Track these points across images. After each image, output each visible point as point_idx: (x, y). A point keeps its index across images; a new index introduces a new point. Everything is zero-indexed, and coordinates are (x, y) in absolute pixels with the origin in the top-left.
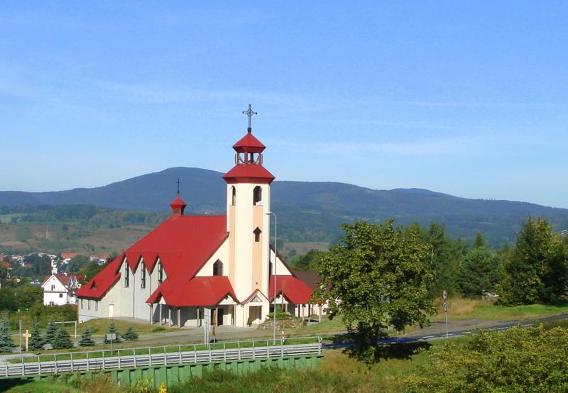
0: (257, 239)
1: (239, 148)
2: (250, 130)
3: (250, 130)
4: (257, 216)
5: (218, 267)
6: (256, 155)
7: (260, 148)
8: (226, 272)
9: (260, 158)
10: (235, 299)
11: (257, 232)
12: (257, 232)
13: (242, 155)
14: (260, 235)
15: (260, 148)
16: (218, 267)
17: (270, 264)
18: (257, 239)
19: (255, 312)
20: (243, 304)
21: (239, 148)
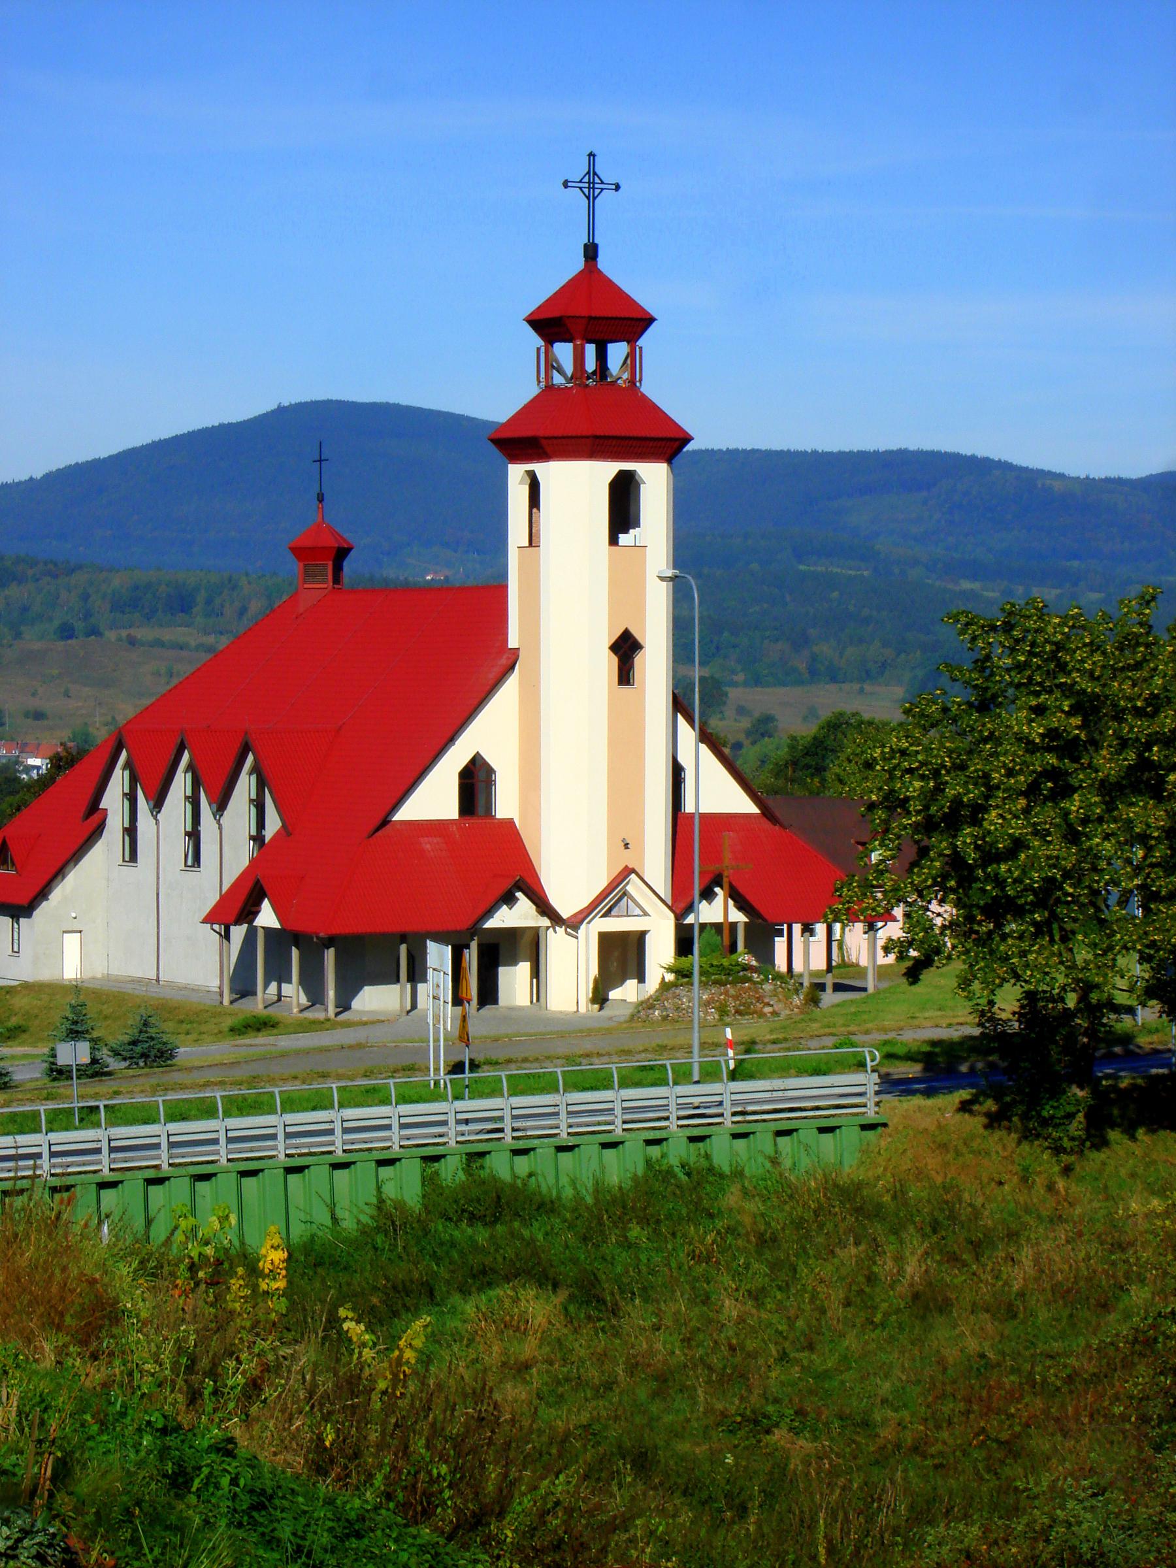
0: (625, 676)
1: (549, 325)
2: (591, 252)
3: (591, 252)
4: (626, 587)
5: (476, 782)
8: (506, 805)
9: (632, 361)
10: (544, 907)
11: (626, 648)
12: (626, 648)
14: (638, 660)
15: (633, 323)
16: (476, 782)
17: (677, 772)
18: (625, 676)
19: (622, 955)
20: (573, 924)
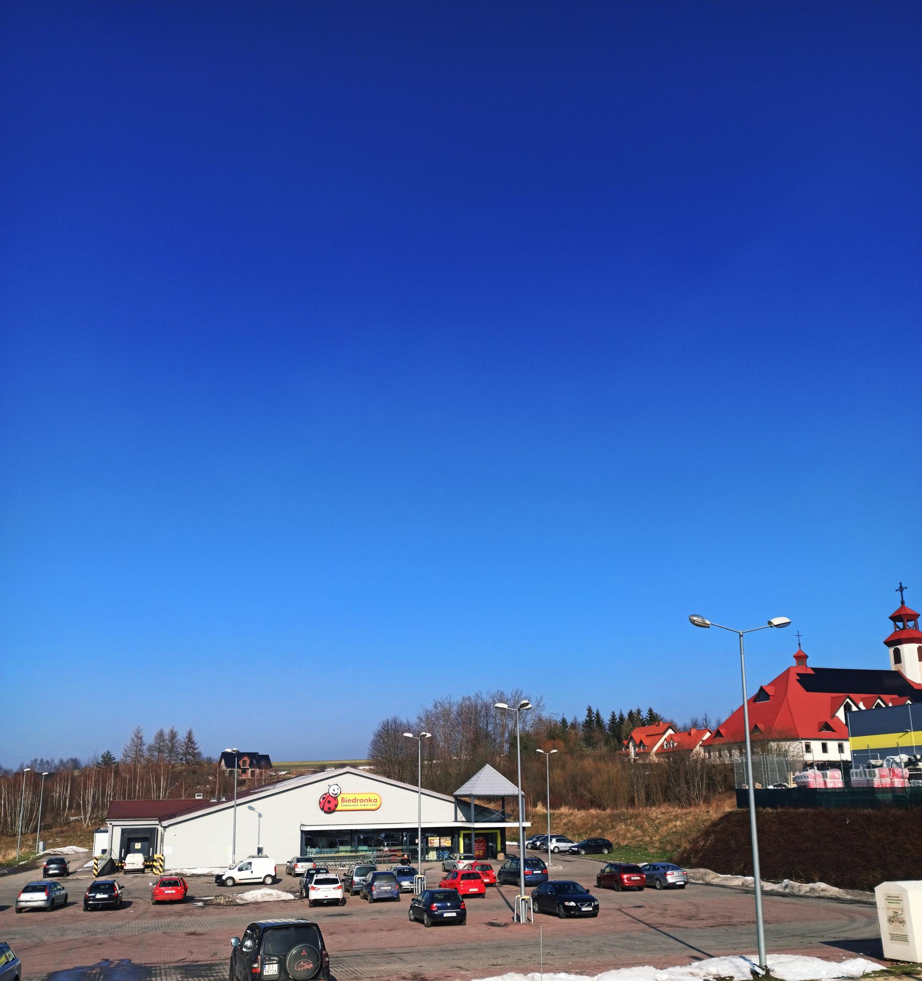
1: (895, 618)
2: (903, 603)
3: (903, 603)
9: (916, 625)
13: (900, 624)
21: (895, 618)
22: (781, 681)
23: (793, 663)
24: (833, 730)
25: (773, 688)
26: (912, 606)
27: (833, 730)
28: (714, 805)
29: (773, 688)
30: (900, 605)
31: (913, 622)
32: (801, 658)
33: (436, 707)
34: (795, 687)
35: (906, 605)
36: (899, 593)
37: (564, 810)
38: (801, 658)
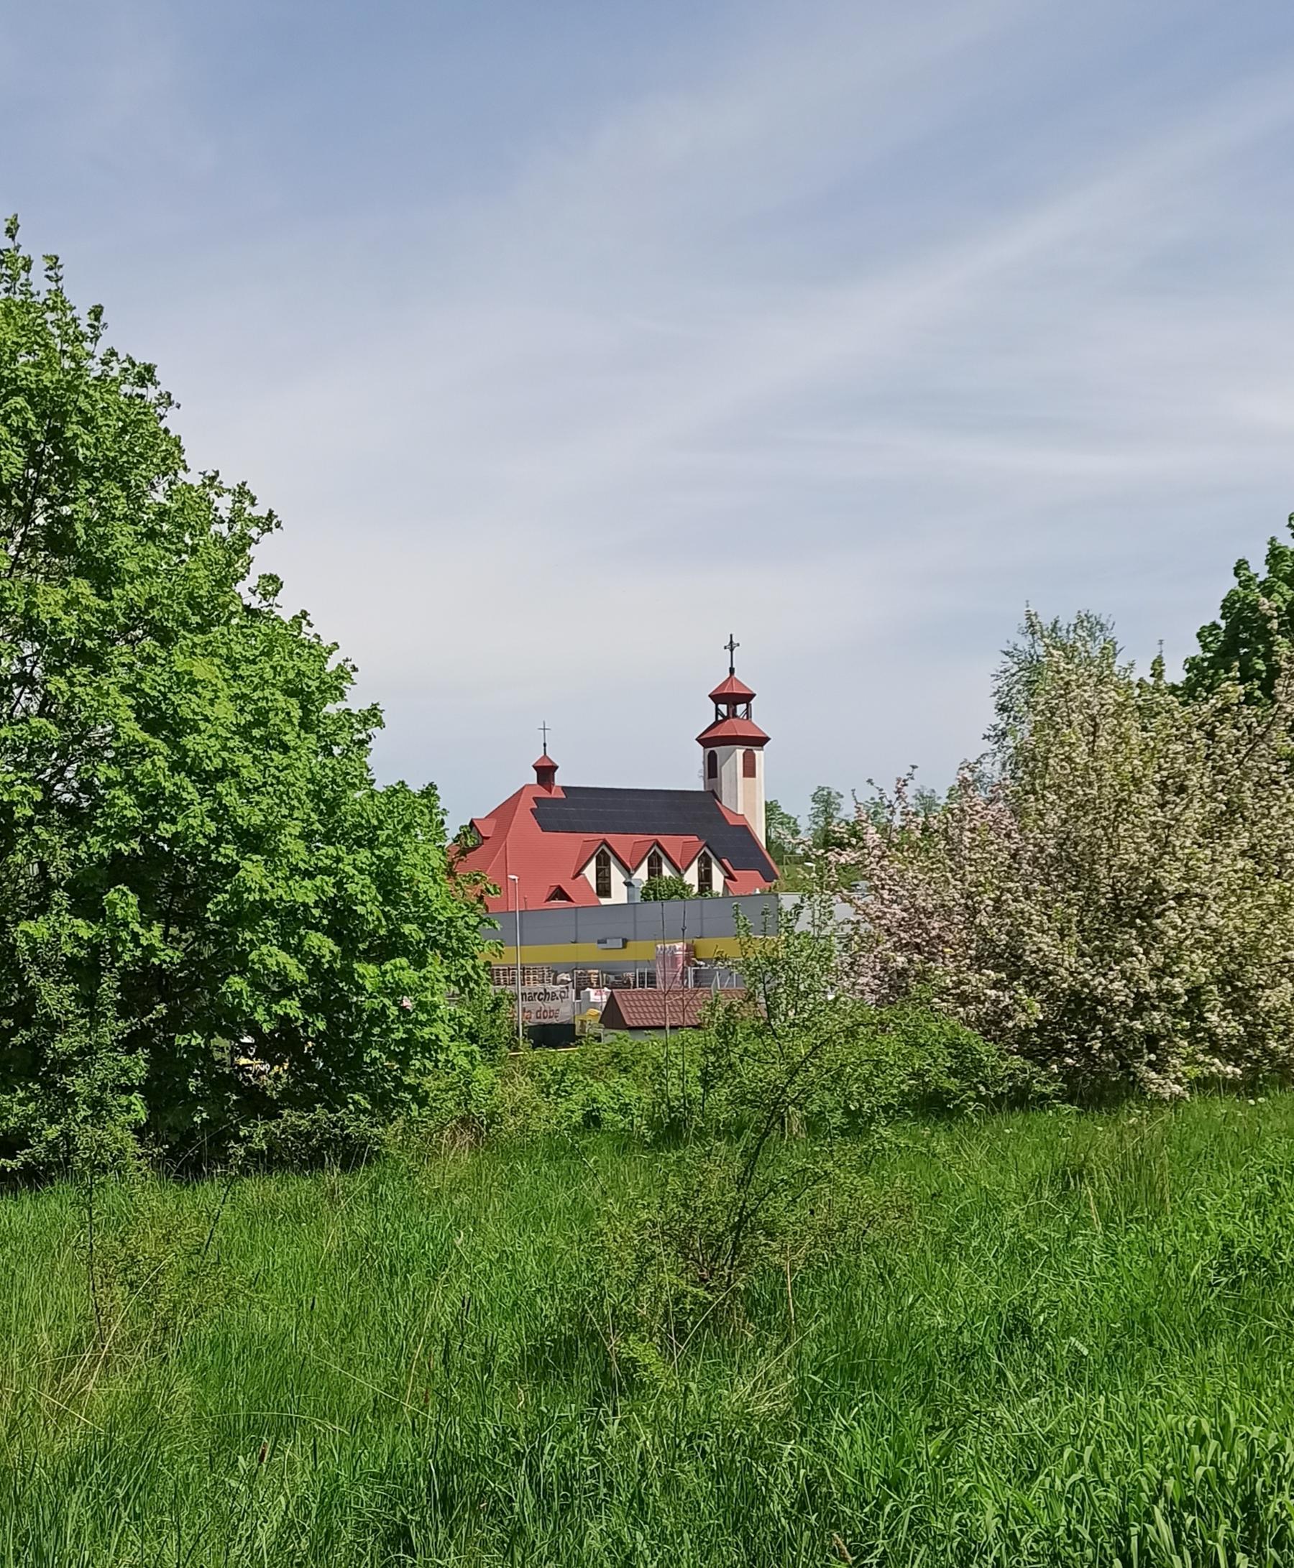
1: (717, 698)
2: (732, 670)
3: (732, 670)
6: (741, 708)
7: (748, 698)
9: (748, 712)
13: (723, 708)
15: (748, 698)
21: (717, 698)
22: (505, 812)
23: (532, 778)
24: (569, 899)
25: (493, 822)
26: (747, 679)
27: (569, 899)
28: (931, 1124)
29: (493, 822)
30: (728, 675)
31: (744, 706)
32: (545, 772)
33: (1205, 647)
34: (524, 819)
35: (736, 675)
36: (728, 651)
37: (79, 922)
38: (545, 772)
